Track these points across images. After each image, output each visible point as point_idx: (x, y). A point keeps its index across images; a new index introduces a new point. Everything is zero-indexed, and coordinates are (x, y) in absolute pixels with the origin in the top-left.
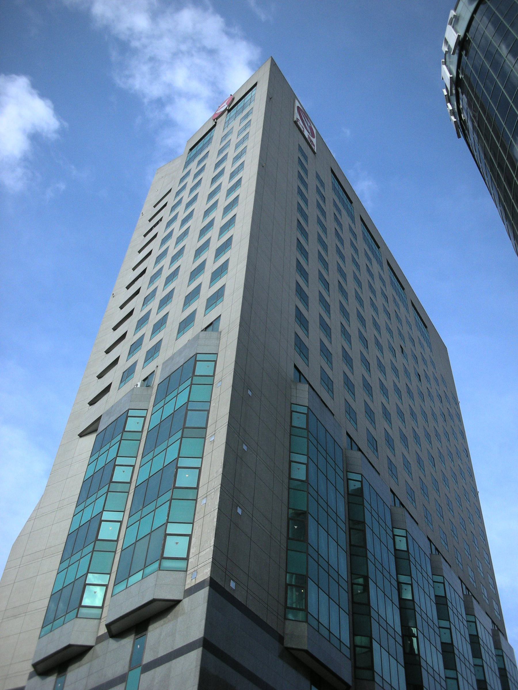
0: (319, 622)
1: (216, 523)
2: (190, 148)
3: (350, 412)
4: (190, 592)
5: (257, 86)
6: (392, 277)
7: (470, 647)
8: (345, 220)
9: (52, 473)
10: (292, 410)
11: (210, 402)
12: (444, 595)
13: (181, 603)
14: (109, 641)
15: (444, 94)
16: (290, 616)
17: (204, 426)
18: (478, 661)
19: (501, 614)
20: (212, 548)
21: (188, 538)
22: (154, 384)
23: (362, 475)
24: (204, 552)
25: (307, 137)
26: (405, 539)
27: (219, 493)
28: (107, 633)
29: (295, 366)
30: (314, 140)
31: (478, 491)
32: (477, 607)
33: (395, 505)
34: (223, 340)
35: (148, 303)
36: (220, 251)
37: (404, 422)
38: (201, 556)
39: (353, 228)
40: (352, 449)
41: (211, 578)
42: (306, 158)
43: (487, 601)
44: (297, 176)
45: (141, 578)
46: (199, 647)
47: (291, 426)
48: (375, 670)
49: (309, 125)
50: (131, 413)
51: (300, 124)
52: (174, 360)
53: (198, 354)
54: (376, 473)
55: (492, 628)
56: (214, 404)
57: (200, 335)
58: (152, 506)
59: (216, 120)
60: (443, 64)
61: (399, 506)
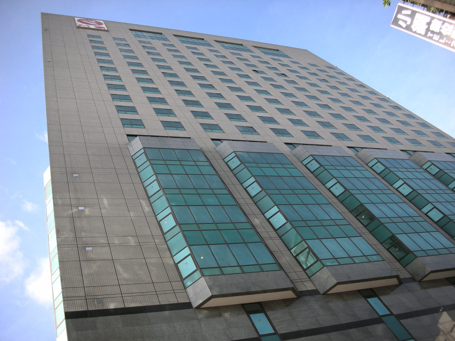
0: (424, 251)
3: (391, 140)
6: (263, 51)
8: (245, 55)
10: (305, 165)
12: (439, 170)
23: (311, 155)
26: (433, 165)
29: (286, 143)
33: (411, 155)
39: (293, 61)
40: (358, 152)
42: (196, 49)
44: (199, 60)
48: (412, 250)
51: (85, 26)
54: (385, 150)
61: (414, 153)
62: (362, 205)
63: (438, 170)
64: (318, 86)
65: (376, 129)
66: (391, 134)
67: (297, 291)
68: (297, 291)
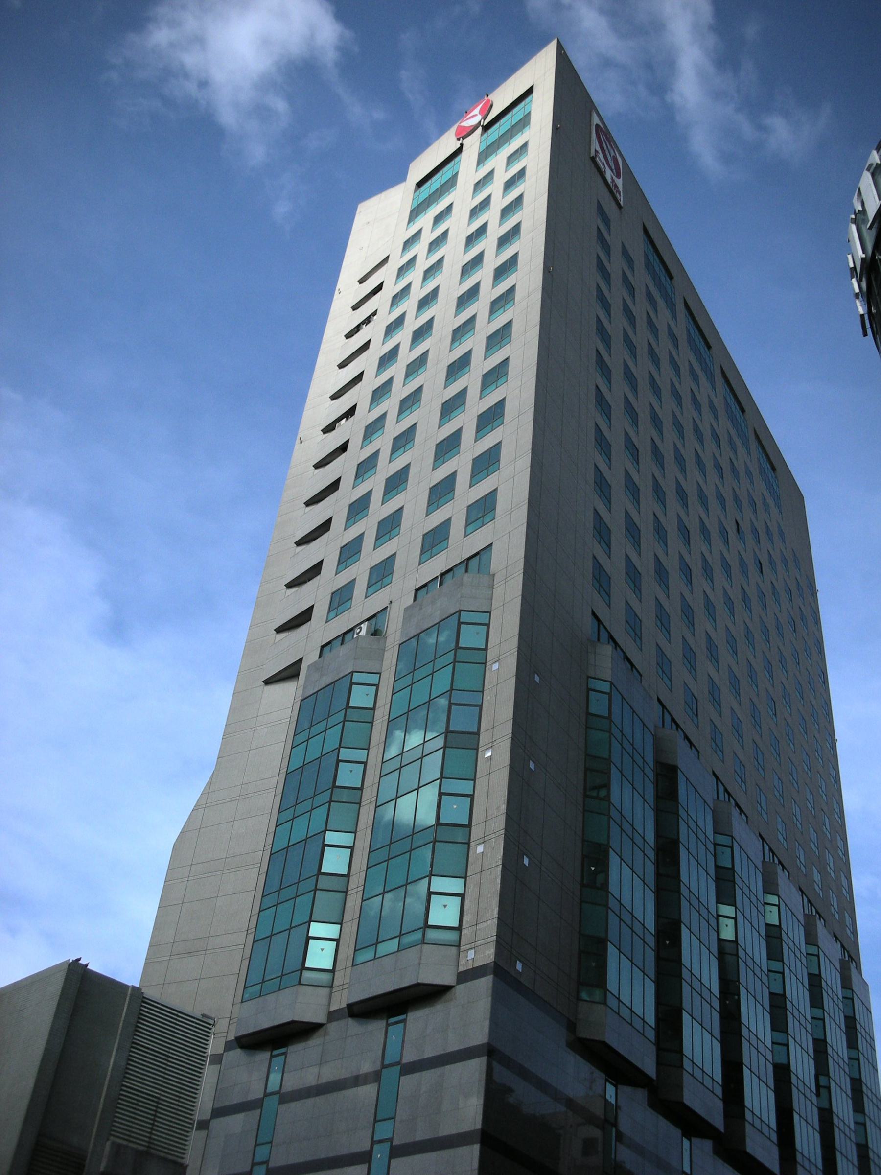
1: (499, 886)
2: (418, 181)
4: (465, 977)
5: (534, 93)
7: (808, 995)
9: (226, 736)
11: (483, 692)
13: (453, 989)
14: (348, 1021)
15: (849, 266)
16: (584, 996)
17: (476, 730)
18: (818, 1013)
19: (855, 932)
20: (496, 921)
21: (459, 899)
22: (388, 632)
24: (485, 924)
25: (609, 180)
27: (503, 842)
28: (346, 1010)
30: (619, 182)
31: (836, 738)
32: (822, 933)
34: (498, 591)
35: (366, 476)
36: (429, 273)
37: (736, 655)
38: (480, 930)
41: (495, 962)
43: (837, 915)
45: (396, 950)
46: (482, 1056)
47: (588, 714)
48: (684, 1053)
49: (612, 154)
50: (357, 678)
51: (600, 160)
52: (424, 609)
53: (462, 612)
55: (841, 958)
56: (489, 697)
57: (464, 580)
58: (322, 726)
59: (461, 139)
60: (852, 223)
62: (608, 761)
63: (730, 866)
64: (657, 337)
65: (633, 531)
66: (645, 565)
67: (613, 1156)
68: (613, 1156)
